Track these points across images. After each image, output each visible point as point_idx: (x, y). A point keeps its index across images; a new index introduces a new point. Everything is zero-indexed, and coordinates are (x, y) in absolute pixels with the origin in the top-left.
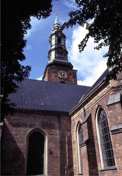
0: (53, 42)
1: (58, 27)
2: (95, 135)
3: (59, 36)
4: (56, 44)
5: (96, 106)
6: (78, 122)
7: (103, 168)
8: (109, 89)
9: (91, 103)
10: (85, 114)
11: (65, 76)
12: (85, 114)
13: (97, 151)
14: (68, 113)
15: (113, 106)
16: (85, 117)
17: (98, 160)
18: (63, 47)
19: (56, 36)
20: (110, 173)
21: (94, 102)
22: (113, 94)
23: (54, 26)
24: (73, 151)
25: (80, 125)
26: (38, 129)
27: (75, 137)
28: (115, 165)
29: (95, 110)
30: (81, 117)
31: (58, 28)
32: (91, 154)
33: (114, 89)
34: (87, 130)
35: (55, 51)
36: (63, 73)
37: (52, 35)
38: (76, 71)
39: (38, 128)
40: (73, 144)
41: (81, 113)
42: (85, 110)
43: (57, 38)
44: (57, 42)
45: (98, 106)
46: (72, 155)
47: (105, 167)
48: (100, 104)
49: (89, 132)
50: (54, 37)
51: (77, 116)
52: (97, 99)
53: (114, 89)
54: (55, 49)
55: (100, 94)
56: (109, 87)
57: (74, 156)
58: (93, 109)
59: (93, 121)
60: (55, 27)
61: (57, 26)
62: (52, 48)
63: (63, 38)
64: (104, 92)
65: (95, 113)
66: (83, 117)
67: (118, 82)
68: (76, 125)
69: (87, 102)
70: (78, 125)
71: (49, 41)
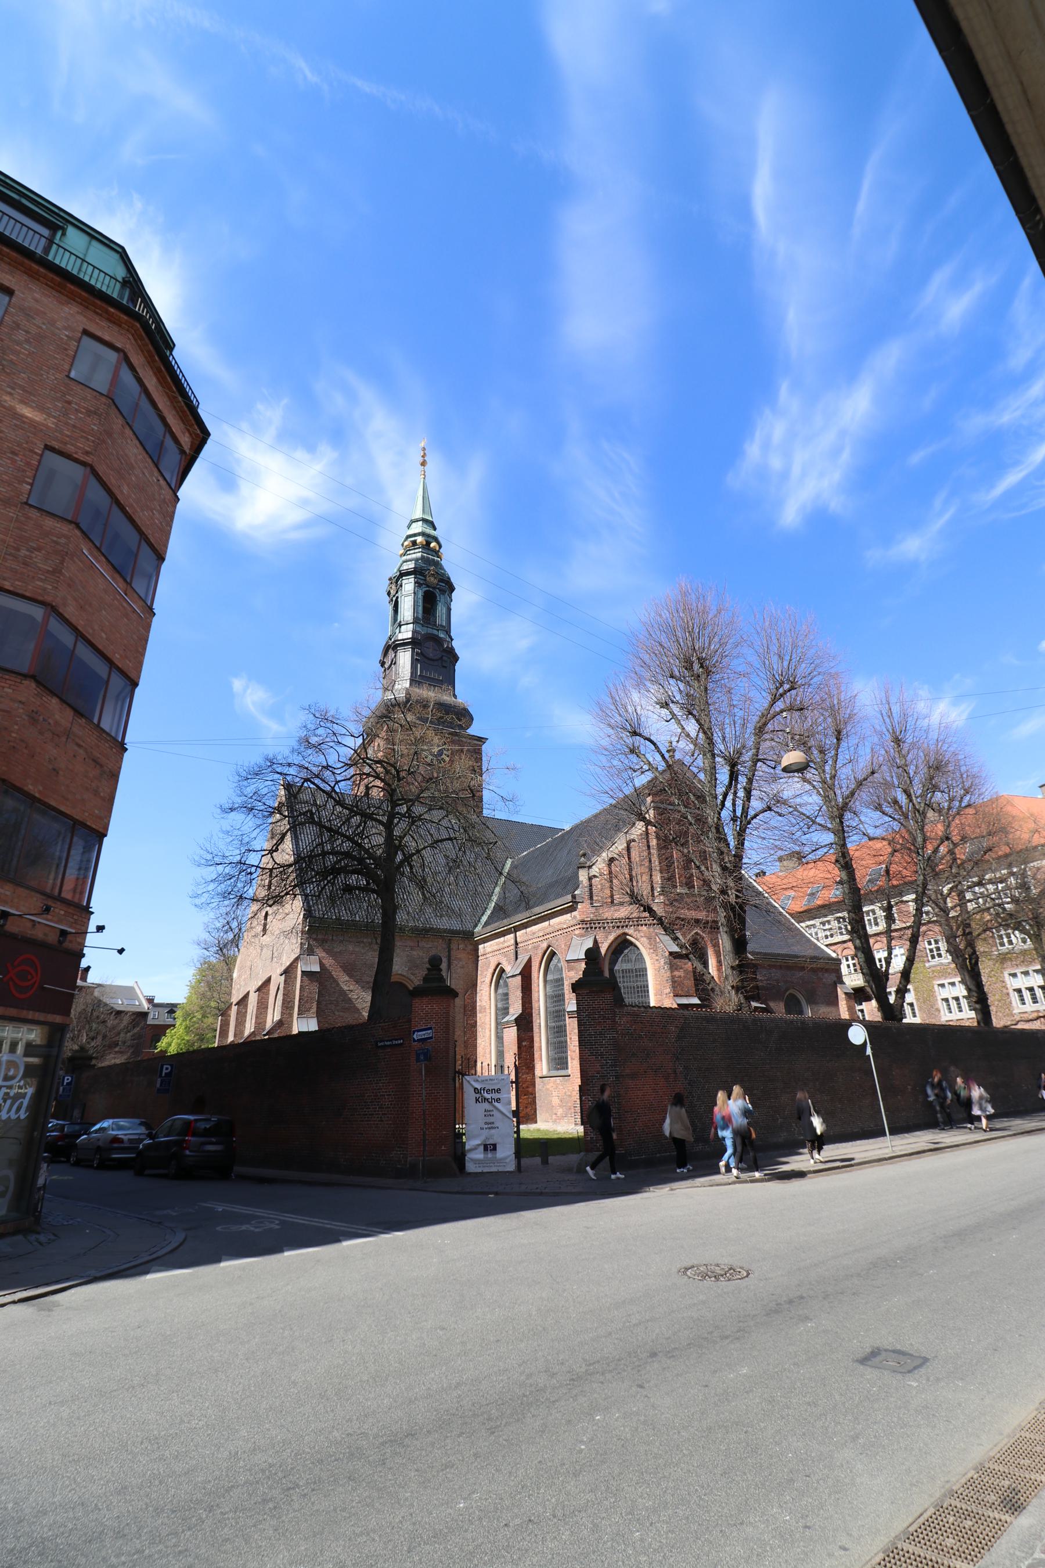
0: (407, 610)
1: (429, 536)
2: (537, 1005)
3: (428, 586)
4: (415, 621)
5: (545, 945)
6: (496, 963)
7: (545, 1072)
8: (575, 922)
9: (534, 933)
10: (516, 952)
11: (444, 756)
12: (516, 952)
13: (536, 1039)
14: (471, 934)
15: (576, 964)
16: (517, 958)
17: (536, 1056)
18: (442, 635)
19: (418, 584)
20: (558, 1082)
21: (541, 934)
22: (581, 936)
23: (409, 527)
24: (479, 1029)
25: (500, 973)
26: (401, 975)
27: (486, 998)
28: (567, 1068)
29: (540, 952)
30: (505, 954)
31: (428, 543)
32: (524, 1044)
33: (584, 926)
34: (519, 994)
35: (413, 649)
36: (439, 746)
37: (402, 574)
38: (482, 740)
39: (400, 972)
40: (480, 1012)
41: (506, 945)
42: (516, 943)
43: (420, 595)
44: (420, 609)
45: (549, 946)
46: (476, 1039)
47: (549, 1070)
48: (553, 942)
49: (523, 998)
50: (409, 585)
51: (495, 948)
52: (548, 931)
53: (584, 926)
54: (414, 643)
55: (554, 921)
56: (575, 917)
57: (479, 1041)
58: (536, 948)
59: (534, 974)
60: (415, 535)
61: (423, 534)
62: (400, 637)
63: (443, 592)
64: (564, 923)
65: (540, 959)
66: (513, 957)
67: (593, 910)
68: (491, 970)
69: (525, 926)
70: (495, 970)
71: (389, 594)
